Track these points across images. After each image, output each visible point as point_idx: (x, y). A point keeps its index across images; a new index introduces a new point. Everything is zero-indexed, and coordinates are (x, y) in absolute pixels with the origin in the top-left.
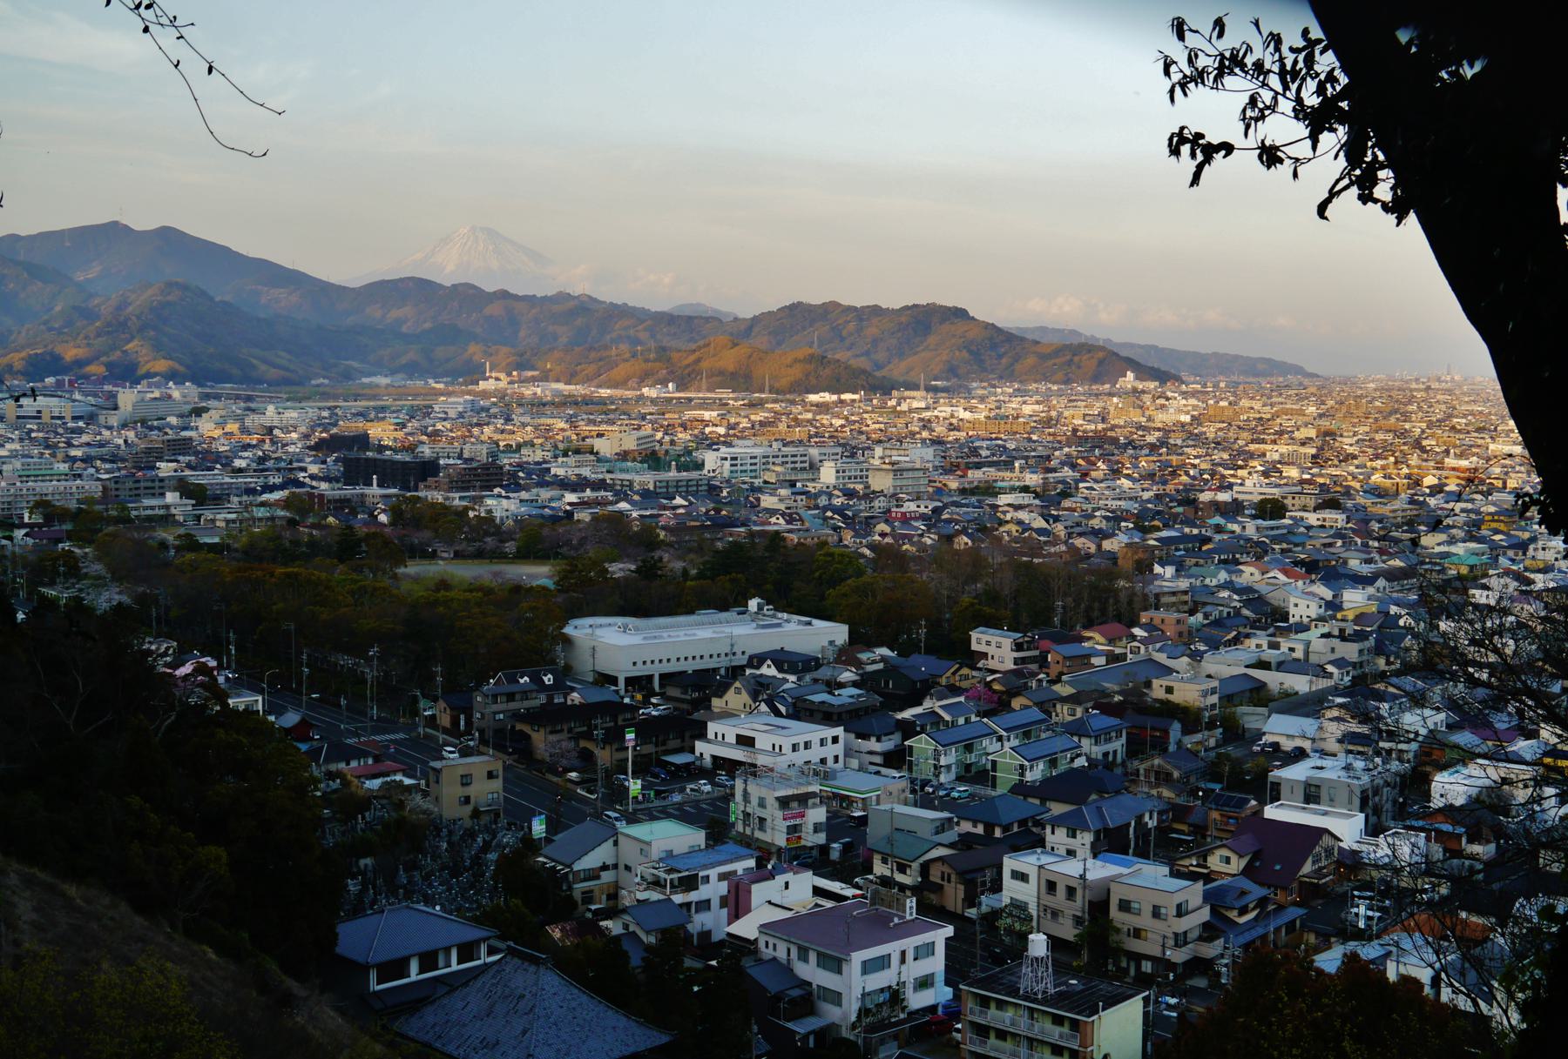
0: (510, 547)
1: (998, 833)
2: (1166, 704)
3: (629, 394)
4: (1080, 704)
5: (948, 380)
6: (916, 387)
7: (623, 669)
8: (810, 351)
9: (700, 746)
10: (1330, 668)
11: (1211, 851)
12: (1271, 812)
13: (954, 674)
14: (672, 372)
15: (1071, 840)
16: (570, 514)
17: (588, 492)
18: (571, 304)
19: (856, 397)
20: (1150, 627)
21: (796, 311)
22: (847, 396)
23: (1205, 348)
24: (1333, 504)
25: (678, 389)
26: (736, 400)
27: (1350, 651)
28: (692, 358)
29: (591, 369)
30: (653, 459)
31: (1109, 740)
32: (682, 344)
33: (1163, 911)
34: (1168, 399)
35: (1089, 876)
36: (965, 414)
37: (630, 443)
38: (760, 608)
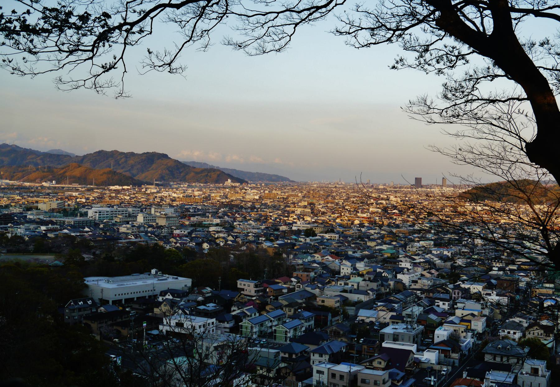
0: (31, 247)
1: (294, 356)
2: (323, 306)
3: (37, 185)
4: (293, 307)
5: (161, 181)
6: (152, 184)
7: (111, 297)
8: (110, 169)
9: (161, 327)
10: (369, 292)
11: (374, 360)
12: (384, 345)
13: (239, 297)
14: (54, 177)
15: (320, 358)
16: (45, 235)
17: (50, 226)
18: (8, 149)
19: (129, 187)
20: (296, 278)
21: (101, 154)
22: (125, 187)
23: (254, 171)
24: (332, 231)
25: (57, 183)
26: (82, 188)
27: (374, 285)
28: (62, 171)
29: (20, 174)
30: (66, 213)
31: (309, 321)
32: (55, 165)
33: (378, 382)
34: (246, 190)
35: (352, 371)
36: (176, 193)
37: (54, 205)
38: (156, 272)
